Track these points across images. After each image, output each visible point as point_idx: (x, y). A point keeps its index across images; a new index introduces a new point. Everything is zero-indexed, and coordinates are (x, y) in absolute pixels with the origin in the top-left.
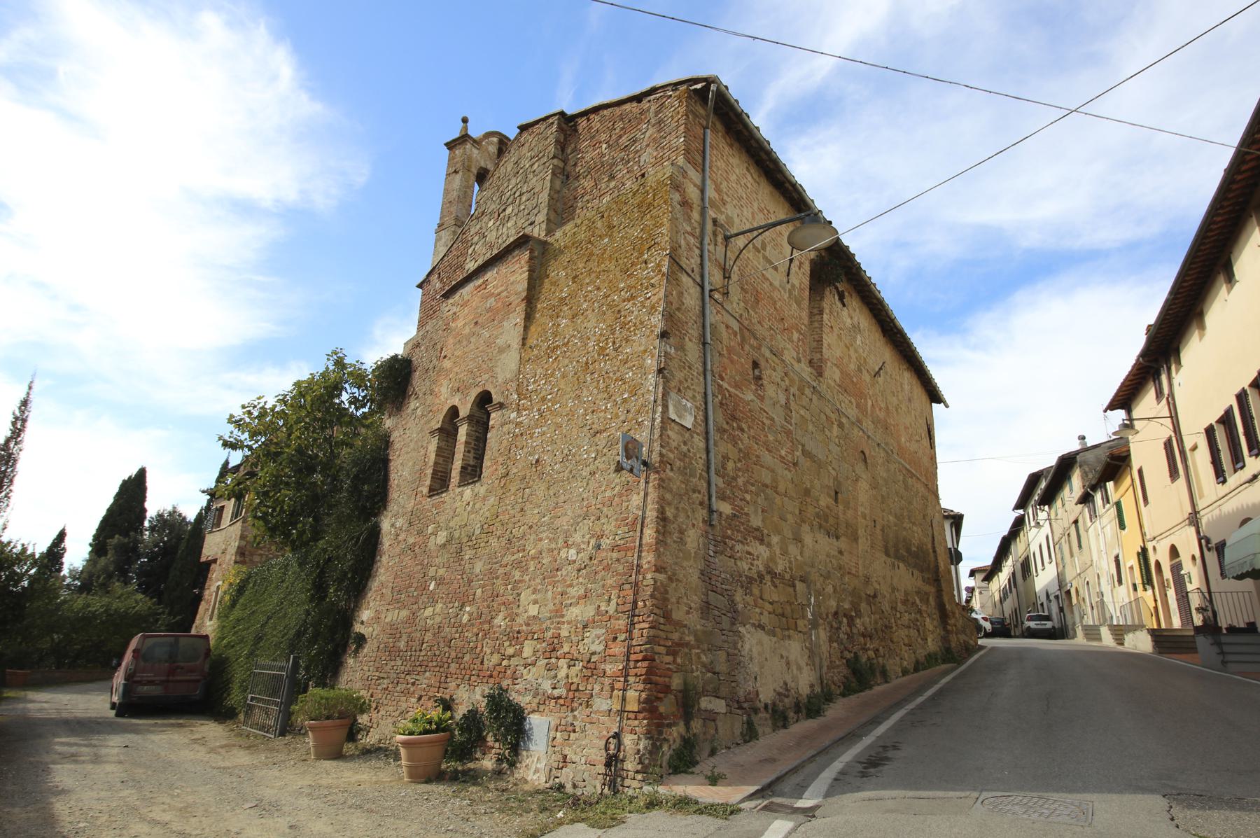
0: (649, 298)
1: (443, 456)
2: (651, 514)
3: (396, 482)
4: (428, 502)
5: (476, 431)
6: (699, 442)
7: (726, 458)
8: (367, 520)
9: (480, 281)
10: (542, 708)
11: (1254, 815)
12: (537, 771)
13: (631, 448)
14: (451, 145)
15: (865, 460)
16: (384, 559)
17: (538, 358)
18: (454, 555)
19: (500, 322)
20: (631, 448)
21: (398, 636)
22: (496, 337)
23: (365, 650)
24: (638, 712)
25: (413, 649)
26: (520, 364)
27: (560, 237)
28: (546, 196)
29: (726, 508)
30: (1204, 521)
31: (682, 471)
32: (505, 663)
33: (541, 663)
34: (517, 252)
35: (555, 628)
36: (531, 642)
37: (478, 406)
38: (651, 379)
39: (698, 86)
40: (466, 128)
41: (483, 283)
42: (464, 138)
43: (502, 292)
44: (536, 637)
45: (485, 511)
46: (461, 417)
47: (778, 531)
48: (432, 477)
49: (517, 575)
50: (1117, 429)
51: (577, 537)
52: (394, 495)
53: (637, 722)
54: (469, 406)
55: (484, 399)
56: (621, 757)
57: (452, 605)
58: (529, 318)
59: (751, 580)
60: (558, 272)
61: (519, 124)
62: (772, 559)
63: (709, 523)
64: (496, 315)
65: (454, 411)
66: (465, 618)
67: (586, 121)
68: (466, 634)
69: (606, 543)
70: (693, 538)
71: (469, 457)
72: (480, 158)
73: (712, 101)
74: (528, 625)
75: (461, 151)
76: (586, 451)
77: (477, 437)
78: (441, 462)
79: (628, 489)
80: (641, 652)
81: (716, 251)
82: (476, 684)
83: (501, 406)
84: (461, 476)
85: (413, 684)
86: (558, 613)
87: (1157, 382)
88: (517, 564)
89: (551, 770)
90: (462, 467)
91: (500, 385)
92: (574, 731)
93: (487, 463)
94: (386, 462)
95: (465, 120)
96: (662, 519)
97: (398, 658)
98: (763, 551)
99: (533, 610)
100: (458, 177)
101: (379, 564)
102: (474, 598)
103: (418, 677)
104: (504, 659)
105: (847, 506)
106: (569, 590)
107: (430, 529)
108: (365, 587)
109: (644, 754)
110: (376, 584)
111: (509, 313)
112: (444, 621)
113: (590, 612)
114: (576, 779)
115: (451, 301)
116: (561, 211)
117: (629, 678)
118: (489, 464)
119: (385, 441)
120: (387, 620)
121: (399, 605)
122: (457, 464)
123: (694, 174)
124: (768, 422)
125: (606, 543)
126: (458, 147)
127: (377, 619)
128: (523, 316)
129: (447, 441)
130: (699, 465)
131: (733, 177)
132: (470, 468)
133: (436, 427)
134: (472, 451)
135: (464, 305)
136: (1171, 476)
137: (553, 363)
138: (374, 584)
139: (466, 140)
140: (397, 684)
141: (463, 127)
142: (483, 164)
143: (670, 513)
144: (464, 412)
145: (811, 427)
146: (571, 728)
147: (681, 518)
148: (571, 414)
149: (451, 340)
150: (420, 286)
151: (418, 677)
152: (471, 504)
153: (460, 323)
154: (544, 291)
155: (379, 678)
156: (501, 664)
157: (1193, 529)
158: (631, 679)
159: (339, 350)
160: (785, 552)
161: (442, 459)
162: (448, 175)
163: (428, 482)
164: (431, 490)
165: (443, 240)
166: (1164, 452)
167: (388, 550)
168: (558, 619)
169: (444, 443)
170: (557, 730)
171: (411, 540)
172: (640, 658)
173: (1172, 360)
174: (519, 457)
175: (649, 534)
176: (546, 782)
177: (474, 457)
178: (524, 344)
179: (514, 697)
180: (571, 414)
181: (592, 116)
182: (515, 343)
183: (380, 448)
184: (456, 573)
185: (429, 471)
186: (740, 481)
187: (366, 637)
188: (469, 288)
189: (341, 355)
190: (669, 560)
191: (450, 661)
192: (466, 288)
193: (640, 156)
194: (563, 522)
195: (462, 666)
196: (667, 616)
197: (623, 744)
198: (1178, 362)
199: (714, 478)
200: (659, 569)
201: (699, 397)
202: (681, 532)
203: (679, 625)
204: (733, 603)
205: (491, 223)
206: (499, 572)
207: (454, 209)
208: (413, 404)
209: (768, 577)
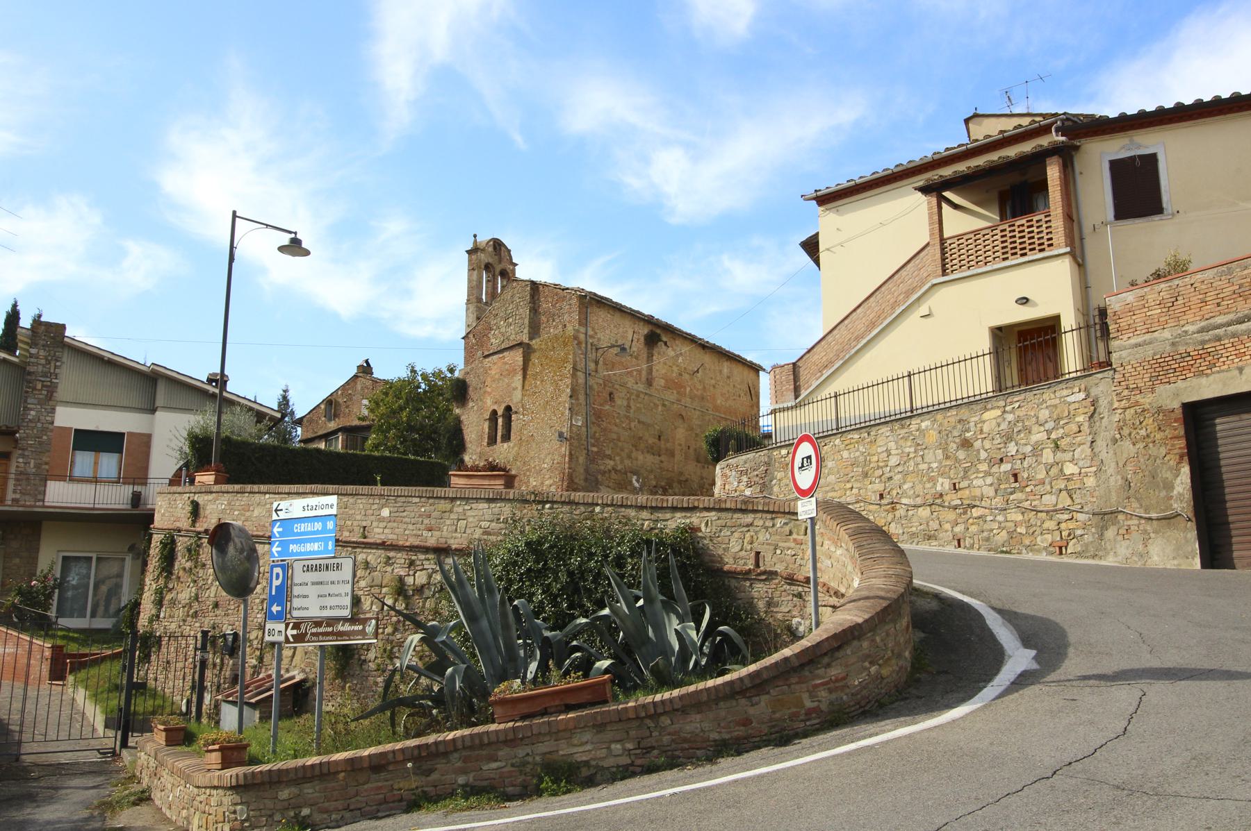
2: (567, 453)
4: (487, 449)
6: (584, 429)
7: (595, 432)
11: (1248, 681)
13: (561, 435)
15: (683, 418)
17: (529, 395)
19: (513, 376)
20: (561, 435)
27: (535, 343)
29: (595, 449)
31: (578, 439)
38: (567, 411)
40: (475, 241)
45: (514, 452)
47: (618, 455)
49: (528, 473)
51: (547, 461)
52: (468, 445)
55: (508, 409)
59: (605, 472)
60: (535, 359)
62: (616, 465)
63: (587, 454)
64: (512, 372)
65: (494, 412)
70: (581, 460)
72: (485, 258)
76: (548, 433)
79: (561, 446)
81: (592, 356)
83: (516, 413)
86: (542, 483)
88: (528, 470)
93: (512, 434)
95: (475, 236)
96: (571, 454)
98: (612, 463)
99: (535, 483)
100: (476, 272)
105: (667, 441)
113: (552, 481)
115: (487, 360)
116: (535, 330)
119: (458, 421)
122: (499, 434)
123: (582, 330)
124: (616, 415)
125: (555, 462)
130: (584, 437)
131: (600, 320)
135: (495, 364)
143: (573, 452)
144: (500, 412)
145: (643, 411)
147: (577, 454)
148: (543, 419)
149: (489, 379)
150: (463, 338)
153: (493, 372)
160: (622, 462)
163: (486, 440)
175: (567, 458)
180: (543, 419)
182: (520, 387)
185: (486, 436)
186: (602, 439)
188: (495, 357)
190: (573, 466)
194: (542, 456)
196: (572, 481)
199: (589, 440)
200: (569, 468)
201: (584, 414)
202: (577, 458)
203: (576, 483)
204: (597, 478)
205: (502, 323)
208: (471, 404)
209: (613, 472)
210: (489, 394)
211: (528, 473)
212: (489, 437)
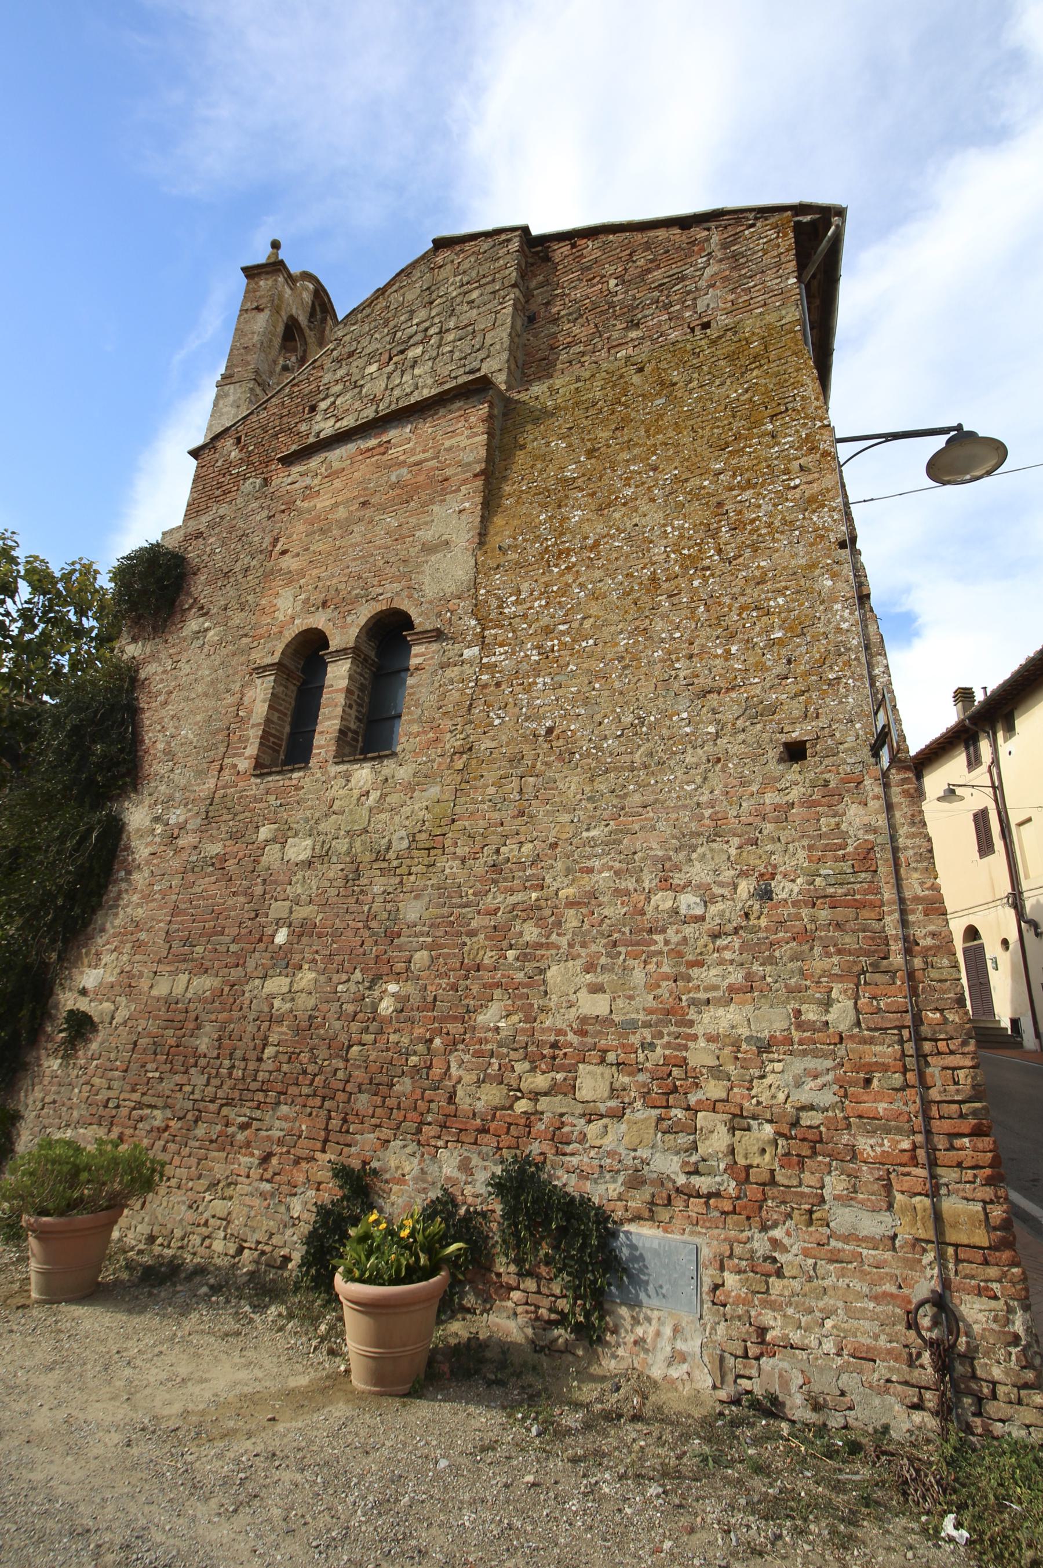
0: (796, 487)
1: (277, 711)
3: (161, 746)
4: (255, 787)
5: (361, 675)
8: (96, 806)
9: (373, 442)
10: (664, 1214)
12: (677, 1357)
14: (251, 272)
16: (139, 878)
18: (340, 883)
21: (191, 1025)
22: (417, 527)
23: (94, 1046)
24: (989, 1248)
25: (239, 1053)
26: (477, 572)
28: (505, 335)
30: (1028, 905)
32: (522, 1106)
33: (639, 1115)
34: (458, 404)
35: (668, 1045)
36: (599, 1069)
37: (367, 633)
39: (807, 219)
41: (380, 445)
42: (275, 267)
43: (426, 460)
44: (611, 1057)
46: (331, 649)
48: (261, 743)
49: (531, 933)
50: (942, 794)
52: (156, 766)
53: (993, 1272)
54: (354, 631)
56: (962, 1347)
57: (344, 977)
58: (490, 504)
61: (435, 237)
66: (386, 1007)
67: (569, 247)
68: (393, 1038)
69: (782, 889)
71: (350, 715)
73: (828, 242)
74: (582, 1033)
75: (270, 282)
77: (362, 684)
78: (275, 719)
80: (961, 1116)
82: (440, 1143)
84: (338, 746)
85: (243, 1127)
87: (972, 748)
89: (722, 1359)
90: (341, 731)
91: (430, 603)
92: (779, 1274)
94: (134, 712)
97: (193, 1070)
101: (124, 886)
102: (408, 969)
103: (257, 1114)
104: (518, 1099)
106: (695, 972)
107: (265, 832)
108: (86, 924)
109: (1028, 1346)
110: (117, 922)
111: (444, 492)
112: (324, 1007)
114: (816, 1388)
117: (940, 1171)
118: (415, 728)
120: (155, 992)
121: (190, 965)
126: (263, 276)
127: (127, 984)
128: (479, 499)
129: (286, 687)
132: (350, 735)
133: (269, 660)
134: (355, 707)
135: (332, 475)
136: (980, 851)
137: (562, 574)
138: (116, 922)
139: (280, 270)
140: (196, 1122)
141: (273, 254)
142: (294, 312)
146: (768, 1267)
150: (195, 453)
151: (257, 1114)
152: (374, 796)
154: (515, 467)
155: (140, 1105)
156: (511, 1107)
157: (1012, 912)
158: (947, 1175)
159: (8, 534)
161: (276, 715)
162: (244, 311)
163: (252, 750)
164: (258, 765)
165: (231, 398)
166: (973, 824)
167: (148, 863)
168: (673, 1029)
169: (282, 688)
170: (722, 1269)
171: (214, 849)
172: (967, 1131)
173: (999, 726)
174: (497, 722)
176: (714, 1387)
177: (357, 718)
178: (481, 544)
179: (566, 1181)
181: (581, 242)
183: (120, 689)
184: (348, 917)
185: (254, 735)
187: (96, 1019)
189: (10, 543)
191: (349, 1088)
192: (337, 452)
193: (695, 299)
195: (391, 1102)
197: (964, 1320)
198: (1010, 729)
206: (474, 924)
207: (253, 358)
210: (290, 578)
211: (531, 933)
212: (265, 737)
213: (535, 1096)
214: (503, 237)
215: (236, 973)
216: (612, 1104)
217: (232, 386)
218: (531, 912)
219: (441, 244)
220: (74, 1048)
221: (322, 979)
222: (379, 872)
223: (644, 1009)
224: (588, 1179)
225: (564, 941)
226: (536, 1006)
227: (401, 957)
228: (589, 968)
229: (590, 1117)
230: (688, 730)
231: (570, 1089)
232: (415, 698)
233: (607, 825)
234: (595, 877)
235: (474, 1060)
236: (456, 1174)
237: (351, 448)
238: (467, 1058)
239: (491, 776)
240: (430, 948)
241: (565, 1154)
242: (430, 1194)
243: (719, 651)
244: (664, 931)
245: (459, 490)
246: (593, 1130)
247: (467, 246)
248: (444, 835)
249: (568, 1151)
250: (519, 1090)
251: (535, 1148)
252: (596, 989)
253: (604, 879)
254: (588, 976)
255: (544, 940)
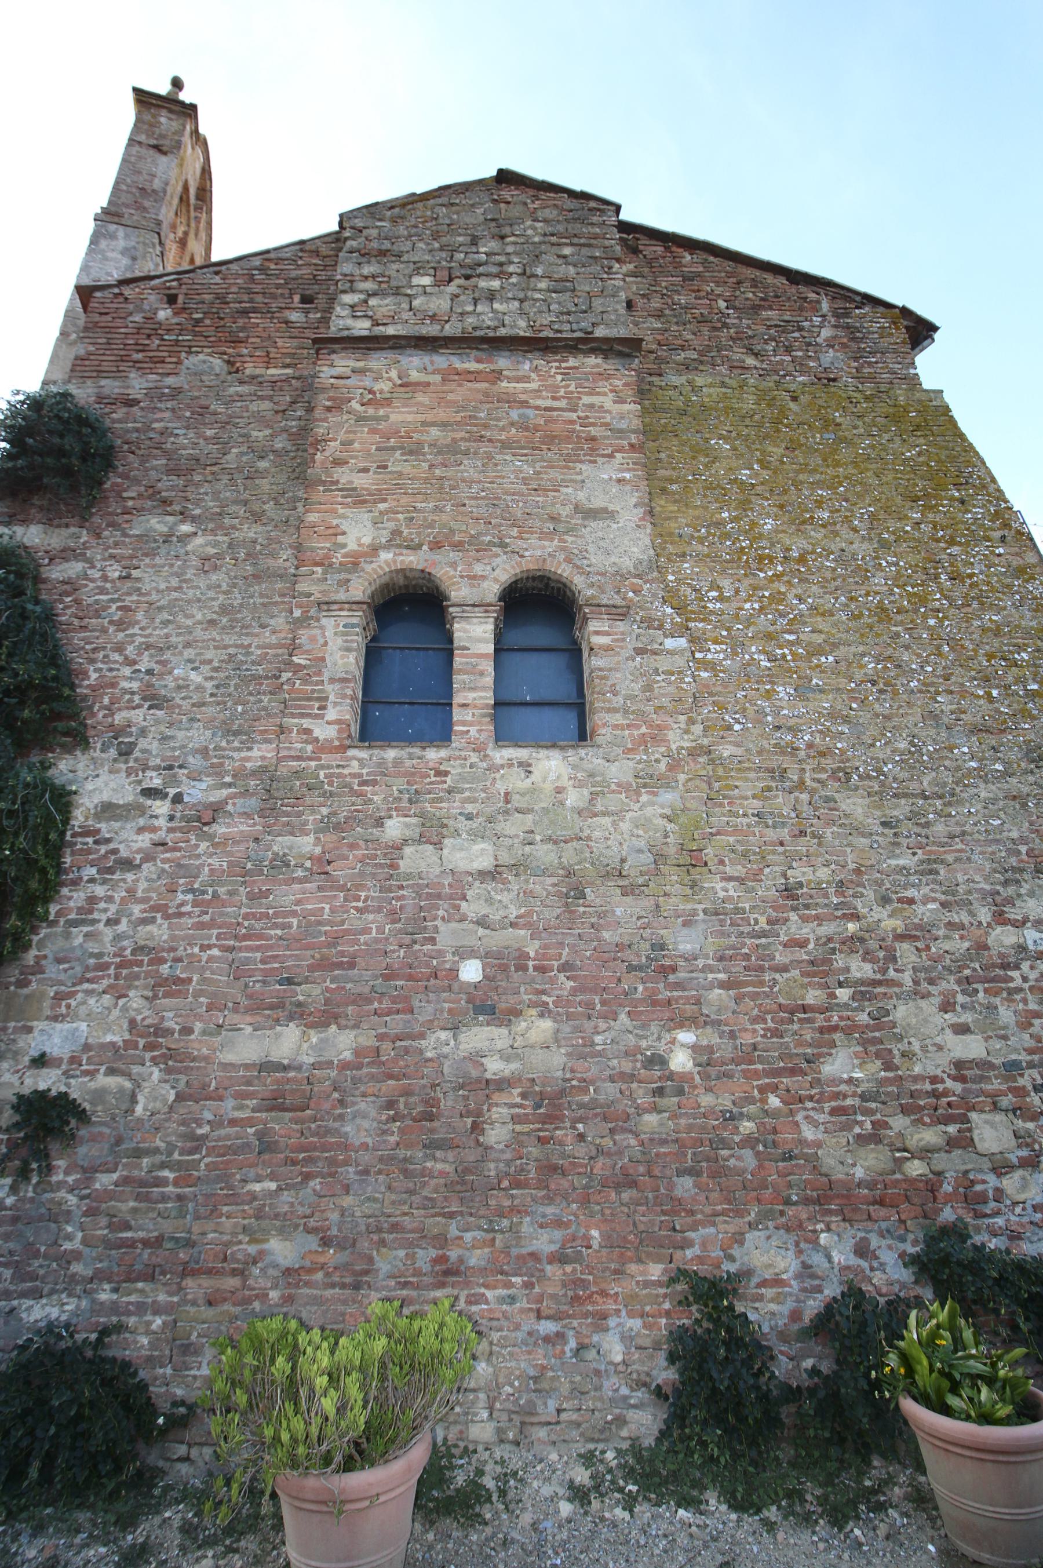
139: (190, 116)
211: (861, 969)
213: (925, 1153)
214: (593, 204)
215: (396, 1023)
216: (1024, 1153)
217: (121, 228)
218: (852, 943)
219: (505, 177)
220: (44, 1156)
221: (566, 1028)
222: (618, 891)
223: (1025, 1050)
224: (1021, 1239)
225: (907, 978)
226: (896, 1052)
227: (687, 998)
228: (947, 1006)
229: (1001, 1168)
230: (973, 764)
231: (964, 1142)
232: (609, 683)
233: (914, 854)
234: (920, 909)
235: (833, 1119)
236: (854, 1261)
237: (441, 360)
238: (821, 1118)
239: (747, 788)
240: (725, 985)
241: (986, 1216)
242: (826, 1292)
243: (981, 693)
244: (1017, 967)
245: (611, 456)
246: (1010, 1184)
247: (543, 195)
248: (701, 850)
249: (989, 1212)
250: (905, 1150)
251: (947, 1215)
252: (962, 1029)
253: (931, 911)
254: (946, 1016)
255: (879, 977)
